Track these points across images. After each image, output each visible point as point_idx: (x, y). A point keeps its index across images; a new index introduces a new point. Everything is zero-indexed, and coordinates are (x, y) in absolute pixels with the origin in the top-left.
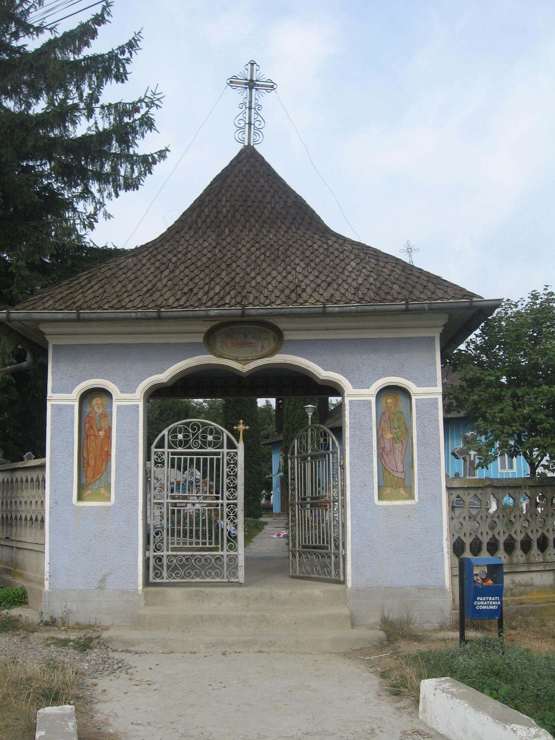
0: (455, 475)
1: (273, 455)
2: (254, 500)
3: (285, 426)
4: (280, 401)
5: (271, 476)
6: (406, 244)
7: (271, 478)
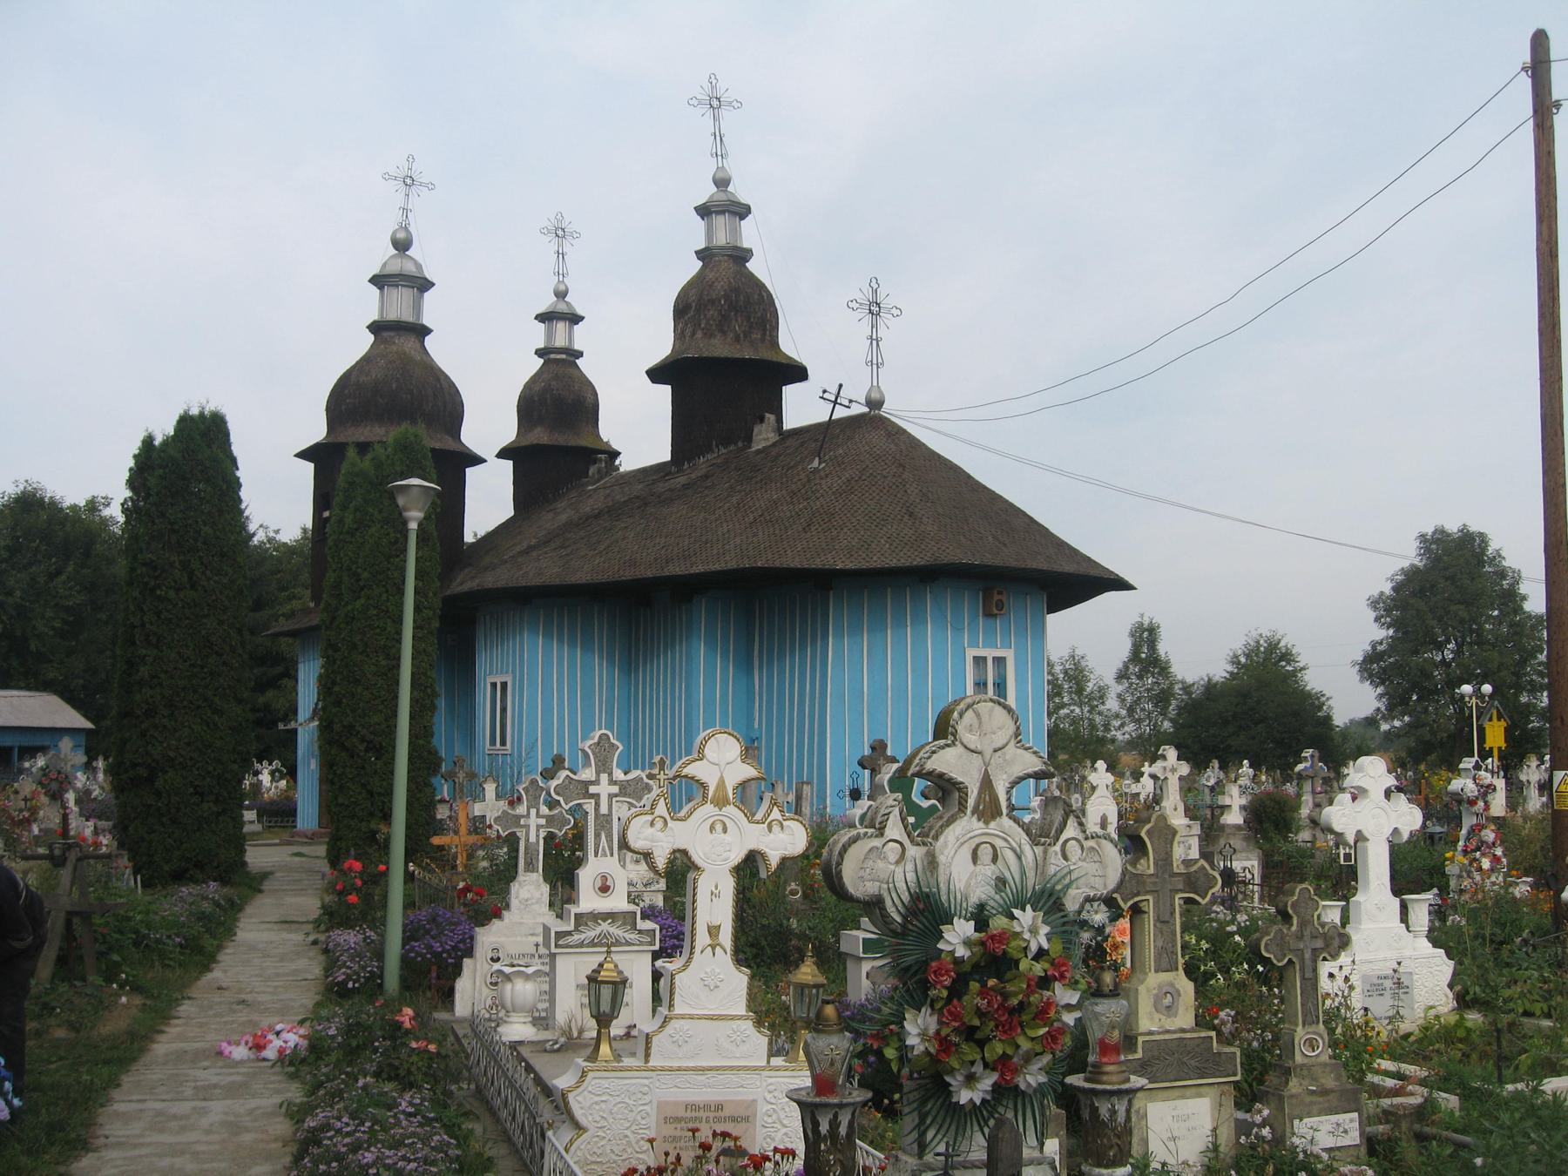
0: (873, 748)
1: (301, 667)
2: (219, 814)
3: (331, 577)
4: (326, 514)
5: (293, 725)
6: (707, 86)
7: (295, 731)
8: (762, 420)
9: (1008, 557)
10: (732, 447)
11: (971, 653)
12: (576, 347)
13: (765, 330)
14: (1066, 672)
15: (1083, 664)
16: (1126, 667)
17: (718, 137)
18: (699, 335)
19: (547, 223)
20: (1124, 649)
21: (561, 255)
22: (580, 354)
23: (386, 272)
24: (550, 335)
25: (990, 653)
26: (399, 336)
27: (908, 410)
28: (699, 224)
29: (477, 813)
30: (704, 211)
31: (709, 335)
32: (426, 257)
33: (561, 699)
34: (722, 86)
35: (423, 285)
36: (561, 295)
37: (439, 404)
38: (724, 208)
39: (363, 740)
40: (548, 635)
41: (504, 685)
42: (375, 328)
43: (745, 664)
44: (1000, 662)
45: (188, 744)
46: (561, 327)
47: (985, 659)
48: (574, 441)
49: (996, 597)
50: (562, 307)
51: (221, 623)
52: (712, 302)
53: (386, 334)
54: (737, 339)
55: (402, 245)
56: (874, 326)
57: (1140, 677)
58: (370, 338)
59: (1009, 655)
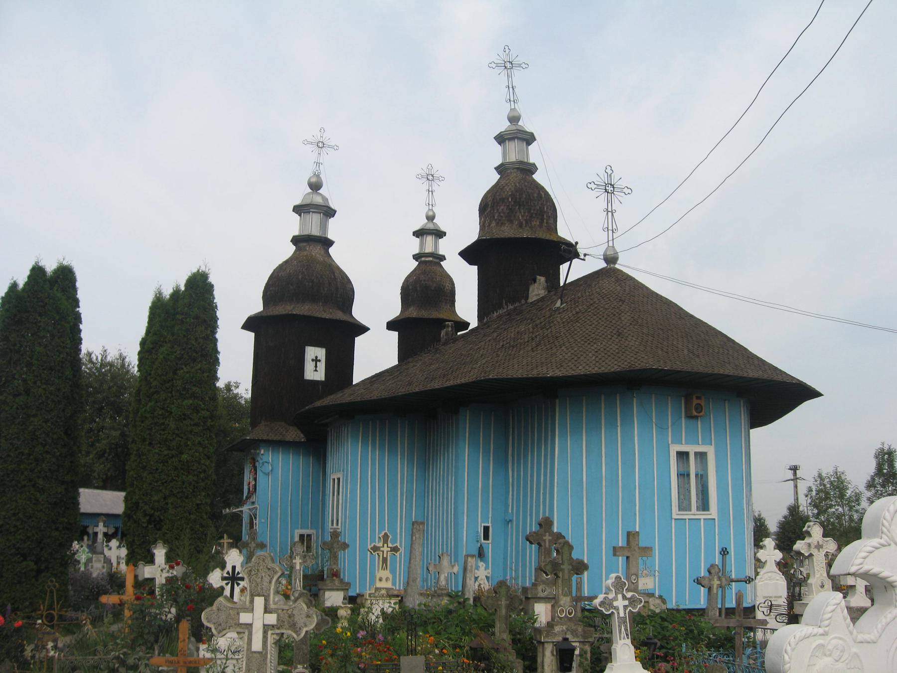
8: (535, 281)
9: (700, 365)
10: (517, 304)
11: (674, 449)
12: (441, 252)
13: (542, 220)
14: (831, 483)
15: (843, 478)
16: (873, 479)
17: (511, 88)
18: (493, 224)
19: (420, 171)
20: (871, 467)
21: (431, 192)
22: (443, 258)
23: (304, 203)
24: (422, 245)
25: (692, 449)
26: (312, 246)
27: (635, 265)
28: (498, 149)
29: (147, 576)
30: (501, 139)
31: (500, 223)
32: (331, 194)
33: (373, 487)
34: (514, 53)
35: (329, 213)
36: (431, 218)
37: (341, 292)
38: (516, 135)
39: (145, 515)
40: (365, 443)
41: (339, 479)
42: (296, 240)
43: (502, 462)
44: (702, 456)
45: (14, 515)
46: (429, 239)
47: (687, 454)
48: (434, 314)
49: (695, 402)
50: (430, 226)
51: (46, 421)
52: (503, 200)
53: (302, 245)
54: (520, 225)
55: (315, 186)
56: (609, 202)
57: (883, 486)
58: (292, 248)
59: (710, 450)
